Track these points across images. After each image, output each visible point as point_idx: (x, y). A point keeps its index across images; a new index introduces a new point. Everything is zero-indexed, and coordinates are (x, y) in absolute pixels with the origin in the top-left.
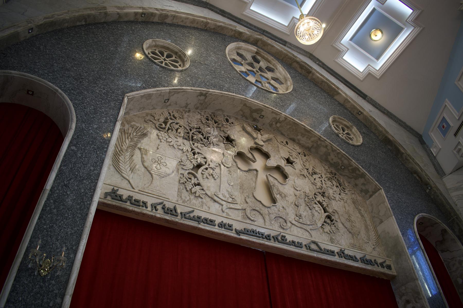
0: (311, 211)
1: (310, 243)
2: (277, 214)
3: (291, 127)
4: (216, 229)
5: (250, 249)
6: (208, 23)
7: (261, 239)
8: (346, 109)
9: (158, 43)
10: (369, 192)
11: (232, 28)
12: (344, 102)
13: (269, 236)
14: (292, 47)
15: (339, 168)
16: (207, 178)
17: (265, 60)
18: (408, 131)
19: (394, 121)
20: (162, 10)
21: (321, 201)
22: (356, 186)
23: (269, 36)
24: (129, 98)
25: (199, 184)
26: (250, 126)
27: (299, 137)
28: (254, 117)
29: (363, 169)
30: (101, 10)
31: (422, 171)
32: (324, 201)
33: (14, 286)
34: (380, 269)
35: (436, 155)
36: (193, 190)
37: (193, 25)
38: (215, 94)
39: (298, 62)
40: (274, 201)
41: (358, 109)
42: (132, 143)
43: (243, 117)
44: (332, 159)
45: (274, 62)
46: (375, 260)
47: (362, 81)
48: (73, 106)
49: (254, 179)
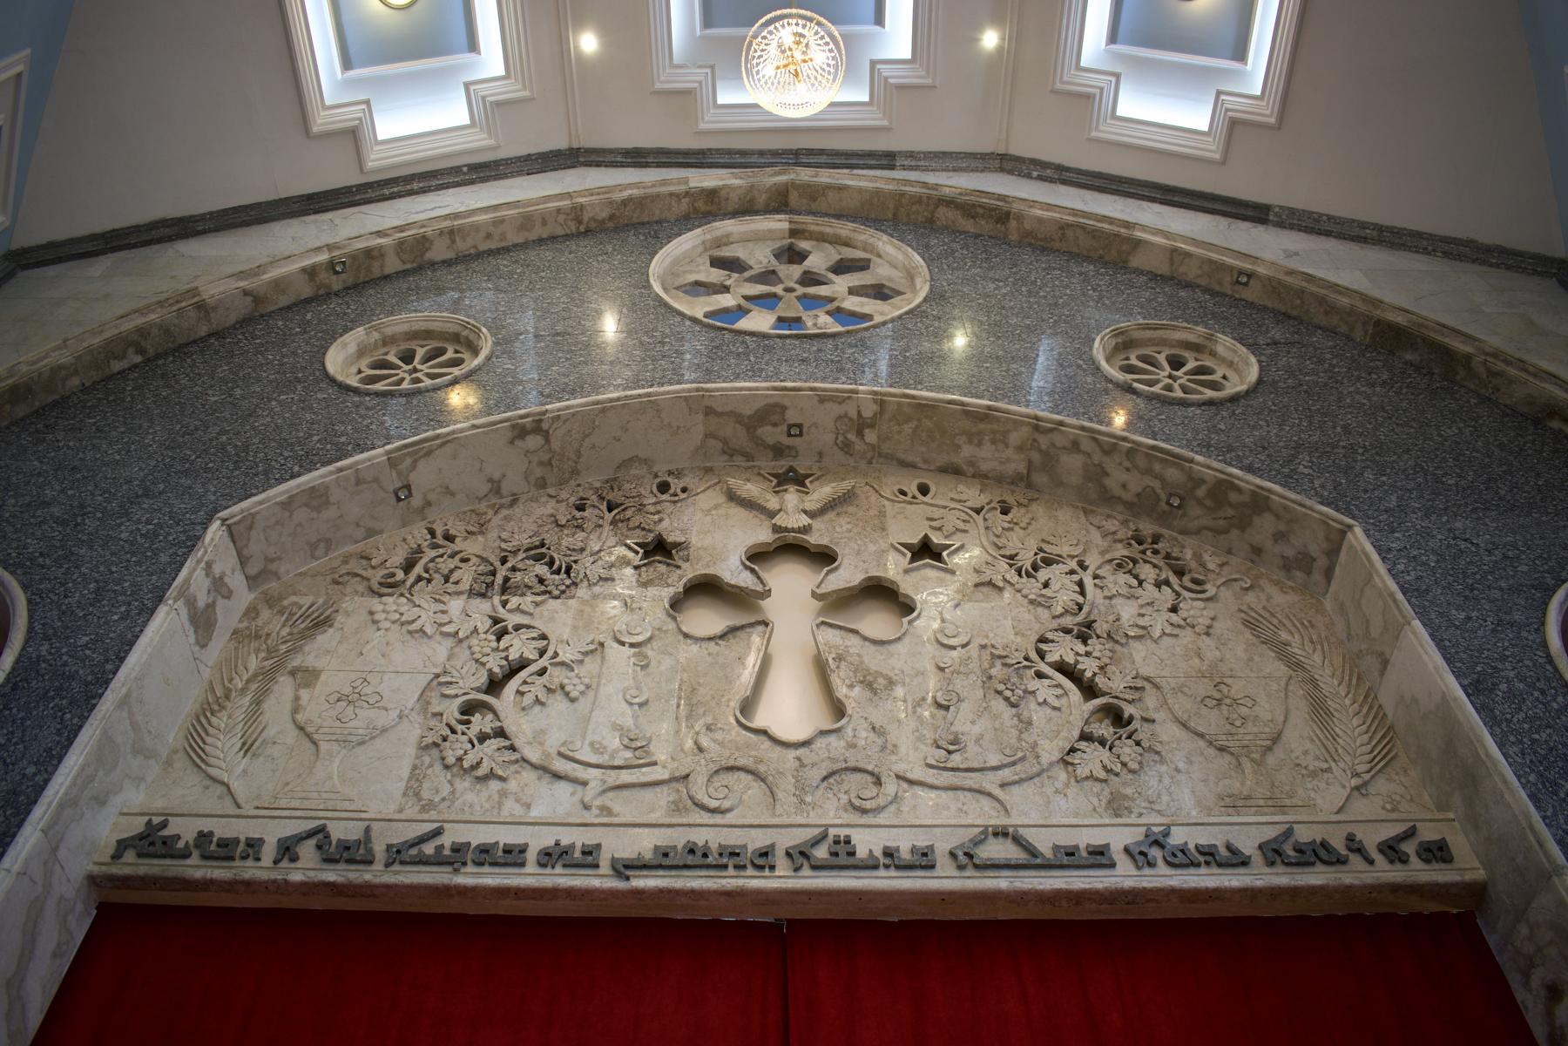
0: (1014, 711)
3: (917, 427)
4: (530, 877)
5: (716, 923)
6: (582, 207)
8: (1188, 285)
9: (389, 331)
10: (1314, 560)
11: (672, 188)
12: (1172, 265)
13: (765, 854)
14: (922, 163)
15: (1164, 512)
17: (830, 243)
18: (1498, 266)
19: (1417, 252)
20: (400, 229)
21: (1070, 659)
22: (1259, 556)
23: (824, 159)
24: (228, 522)
26: (764, 477)
27: (967, 451)
28: (770, 441)
29: (1250, 477)
30: (181, 302)
32: (1088, 654)
34: (1385, 872)
37: (533, 236)
38: (574, 415)
39: (949, 203)
41: (1231, 268)
43: (732, 456)
44: (1124, 486)
45: (863, 237)
46: (1350, 838)
47: (1224, 162)
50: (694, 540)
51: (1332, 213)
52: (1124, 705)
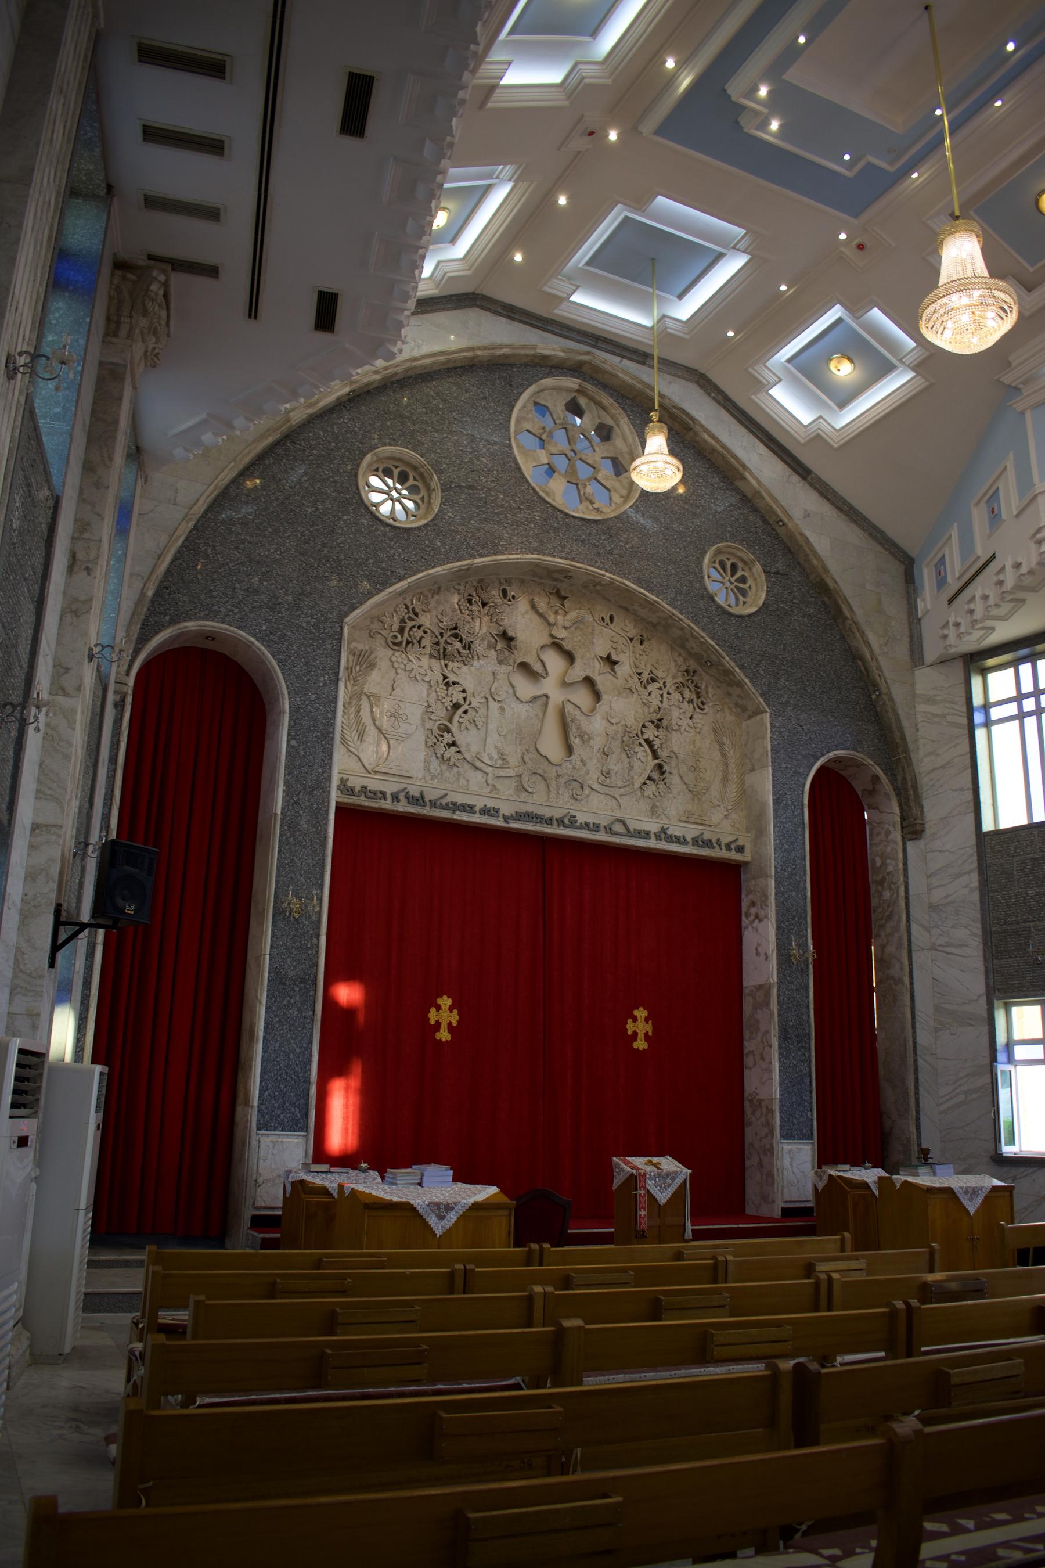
0: (628, 760)
1: (612, 823)
2: (569, 776)
7: (539, 824)
16: (467, 728)
25: (454, 744)
31: (872, 658)
33: (273, 932)
35: (922, 617)
36: (447, 756)
40: (569, 750)
42: (356, 688)
46: (718, 840)
48: (279, 666)
49: (540, 714)
50: (518, 635)
51: (836, 489)
52: (664, 764)
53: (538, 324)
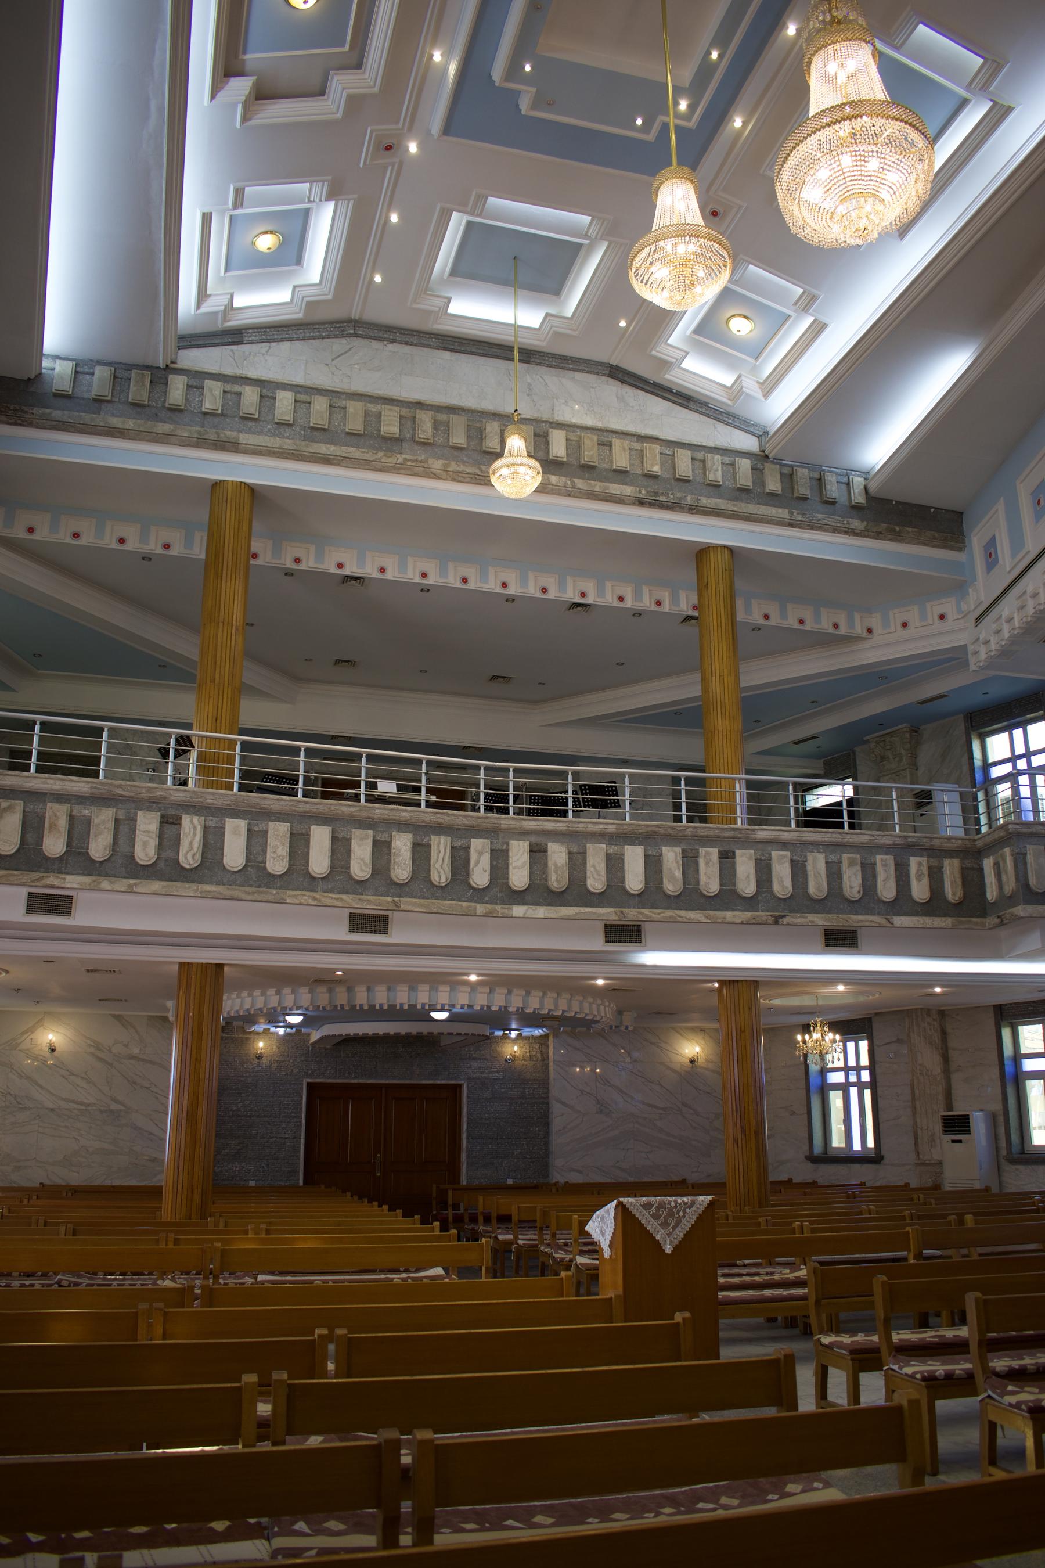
53: (676, 400)
